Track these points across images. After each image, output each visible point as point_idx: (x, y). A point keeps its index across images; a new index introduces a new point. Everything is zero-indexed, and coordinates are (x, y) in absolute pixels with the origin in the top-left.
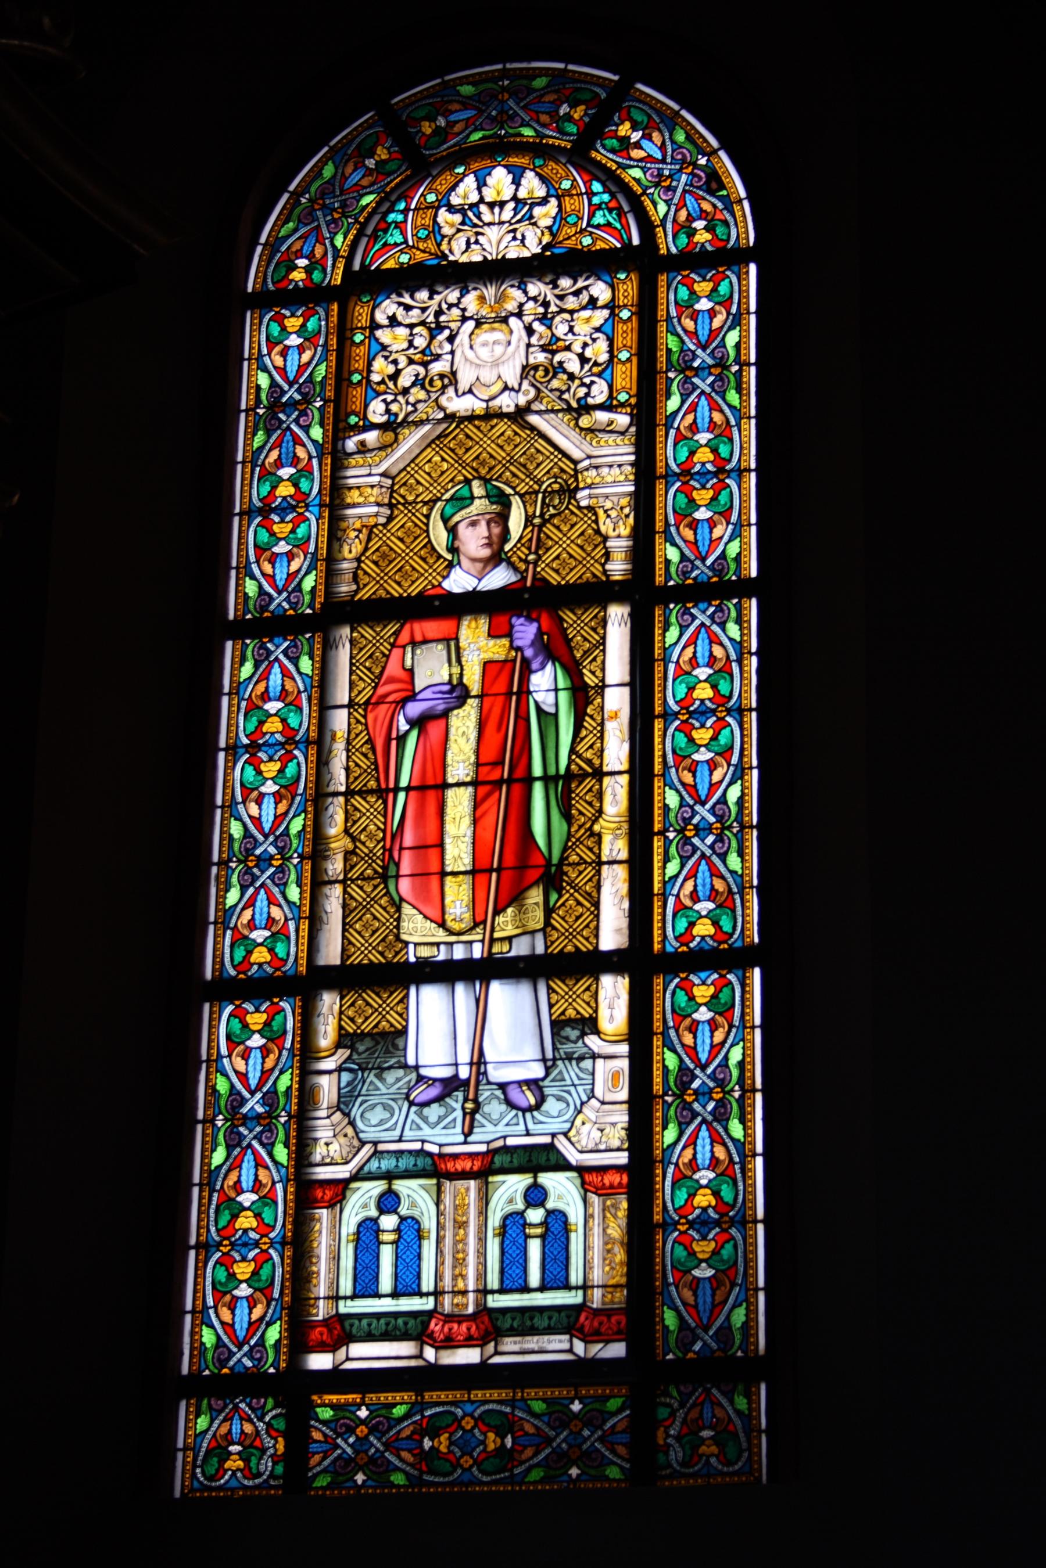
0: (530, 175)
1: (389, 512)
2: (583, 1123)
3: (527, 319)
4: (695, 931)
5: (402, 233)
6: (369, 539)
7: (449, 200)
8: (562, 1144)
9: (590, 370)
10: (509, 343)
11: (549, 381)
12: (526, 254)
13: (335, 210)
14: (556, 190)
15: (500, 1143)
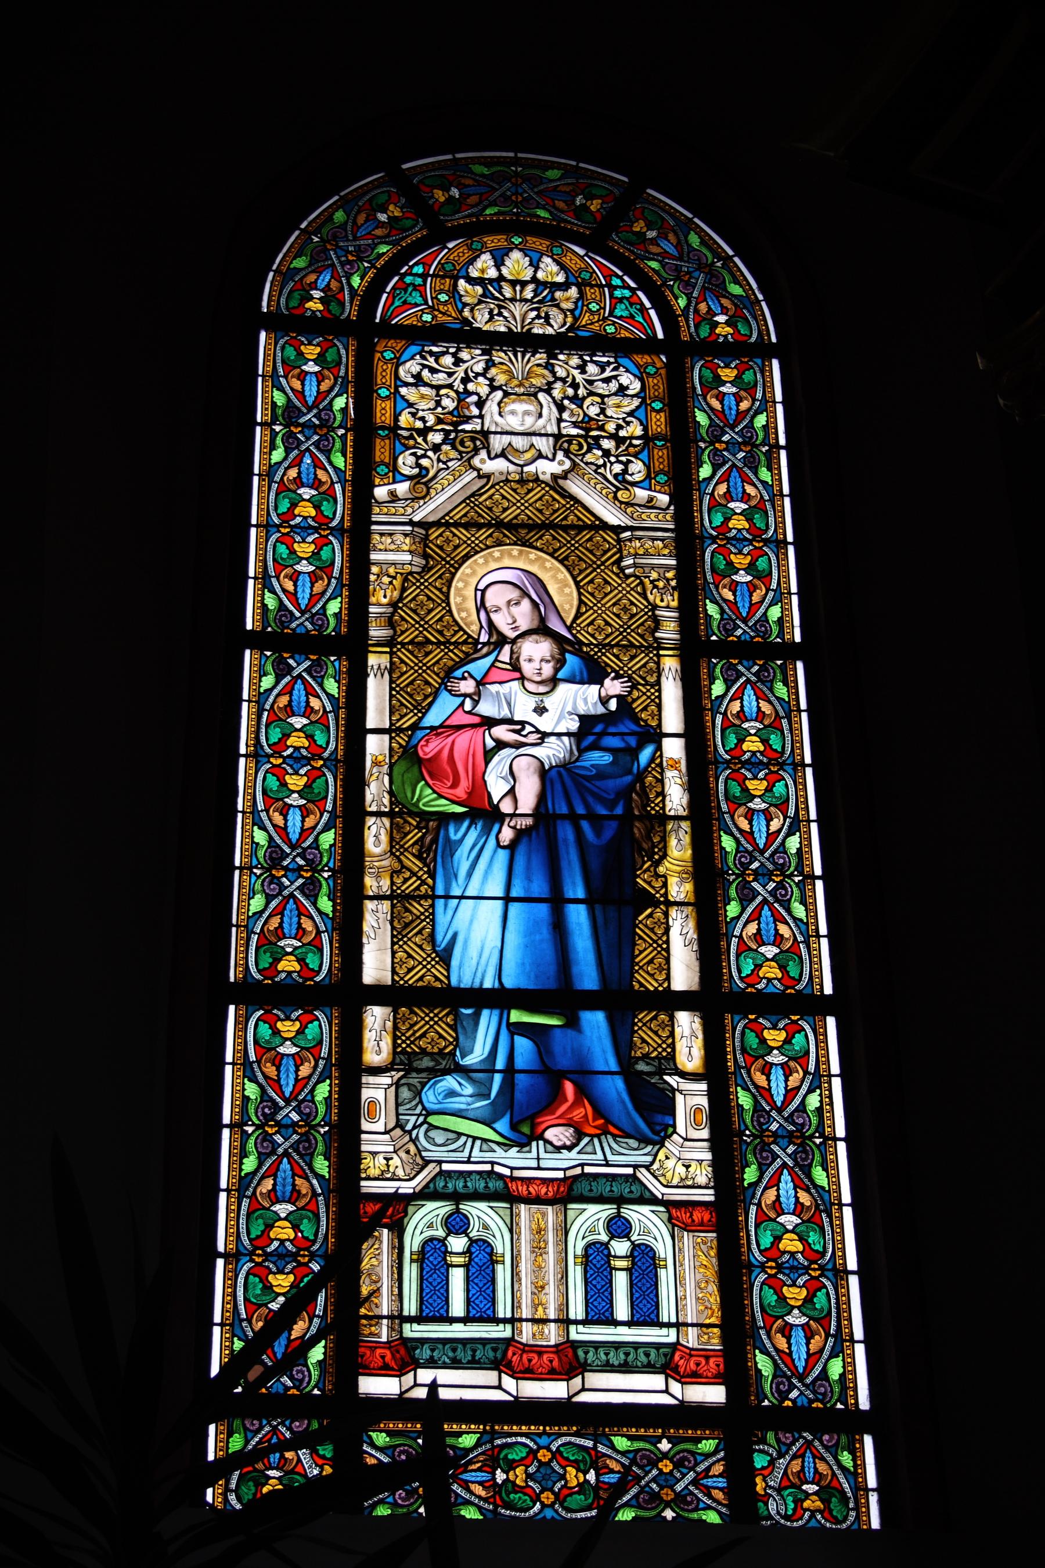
0: (547, 260)
1: (424, 562)
2: (667, 1158)
3: (557, 393)
4: (783, 1035)
5: (421, 296)
6: (404, 589)
7: (468, 273)
8: (644, 1175)
9: (627, 449)
10: (540, 416)
11: (584, 455)
12: (549, 331)
13: (351, 253)
14: (576, 278)
15: (578, 1171)
